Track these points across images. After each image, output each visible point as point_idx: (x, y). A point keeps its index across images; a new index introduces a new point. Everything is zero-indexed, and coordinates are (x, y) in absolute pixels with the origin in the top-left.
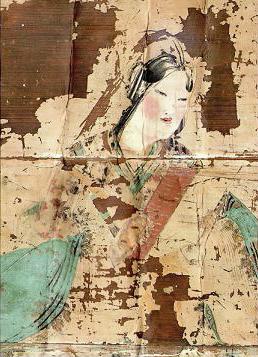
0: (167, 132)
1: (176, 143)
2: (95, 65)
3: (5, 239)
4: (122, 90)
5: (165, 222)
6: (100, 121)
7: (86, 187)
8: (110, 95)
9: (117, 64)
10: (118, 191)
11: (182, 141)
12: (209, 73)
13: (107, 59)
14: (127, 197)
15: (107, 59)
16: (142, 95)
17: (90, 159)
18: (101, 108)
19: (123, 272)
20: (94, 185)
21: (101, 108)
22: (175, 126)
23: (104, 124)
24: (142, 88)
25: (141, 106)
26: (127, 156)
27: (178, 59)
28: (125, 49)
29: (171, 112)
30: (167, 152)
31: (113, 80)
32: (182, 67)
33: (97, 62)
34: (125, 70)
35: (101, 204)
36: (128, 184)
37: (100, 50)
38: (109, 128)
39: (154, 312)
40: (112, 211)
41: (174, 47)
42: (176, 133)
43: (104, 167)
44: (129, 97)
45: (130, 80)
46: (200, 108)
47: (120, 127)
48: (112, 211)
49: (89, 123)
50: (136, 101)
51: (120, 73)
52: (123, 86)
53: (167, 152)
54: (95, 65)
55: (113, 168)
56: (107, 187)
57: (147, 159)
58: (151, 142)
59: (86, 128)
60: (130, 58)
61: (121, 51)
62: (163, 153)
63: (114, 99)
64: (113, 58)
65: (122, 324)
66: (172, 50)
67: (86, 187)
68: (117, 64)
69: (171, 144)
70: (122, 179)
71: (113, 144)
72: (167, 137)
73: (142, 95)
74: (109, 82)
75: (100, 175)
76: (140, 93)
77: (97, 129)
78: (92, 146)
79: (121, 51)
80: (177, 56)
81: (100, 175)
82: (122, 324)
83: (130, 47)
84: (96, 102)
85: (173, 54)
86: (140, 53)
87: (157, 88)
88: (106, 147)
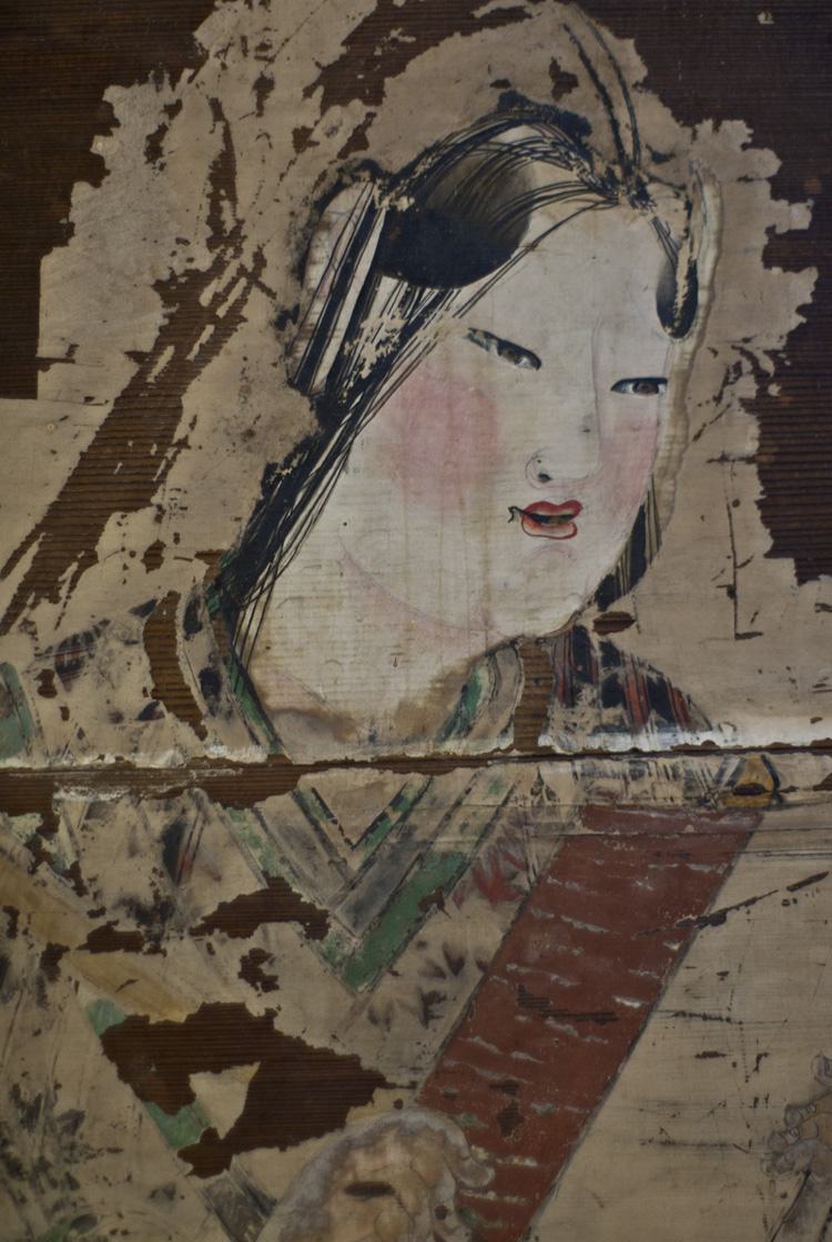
0: (552, 592)
1: (612, 655)
2: (81, 191)
3: (113, 1239)
4: (254, 336)
5: (558, 1145)
6: (122, 534)
7: (53, 956)
8: (182, 372)
9: (223, 175)
10: (254, 970)
11: (657, 641)
12: (798, 216)
13: (154, 150)
14: (307, 1008)
15: (154, 150)
16: (383, 367)
17: (76, 778)
18: (127, 457)
19: (251, 833)
20: (103, 940)
21: (127, 457)
22: (597, 550)
23: (153, 557)
24: (384, 318)
25: (377, 428)
26: (304, 748)
27: (601, 138)
28: (264, 86)
29: (571, 466)
30: (557, 712)
31: (198, 279)
32: (622, 181)
33: (95, 171)
34: (267, 200)
35: (155, 1057)
36: (315, 925)
37: (112, 94)
38: (185, 576)
39: (40, 688)
40: (221, 1096)
41: (570, 63)
42: (608, 591)
43: (158, 822)
44: (300, 381)
45: (299, 271)
46: (746, 436)
47: (244, 571)
48: (221, 1096)
49: (67, 536)
50: (340, 404)
51: (235, 238)
52: (258, 311)
53: (557, 712)
54: (81, 191)
55: (213, 828)
56: (182, 950)
57: (438, 765)
58: (454, 658)
59: (42, 584)
60: (302, 138)
61: (239, 100)
62: (531, 720)
63: (204, 400)
64: (192, 142)
65: (275, 294)
66: (564, 82)
67: (53, 956)
68: (223, 175)
69: (583, 667)
70: (274, 902)
71: (210, 680)
72: (550, 621)
73: (383, 367)
74: (178, 291)
75: (137, 878)
76: (369, 353)
77: (106, 587)
78: (83, 696)
79: (239, 100)
80: (596, 116)
81: (137, 878)
82: (275, 294)
83: (294, 73)
84: (98, 414)
85: (566, 104)
86: (358, 108)
87: (481, 317)
88: (168, 695)
